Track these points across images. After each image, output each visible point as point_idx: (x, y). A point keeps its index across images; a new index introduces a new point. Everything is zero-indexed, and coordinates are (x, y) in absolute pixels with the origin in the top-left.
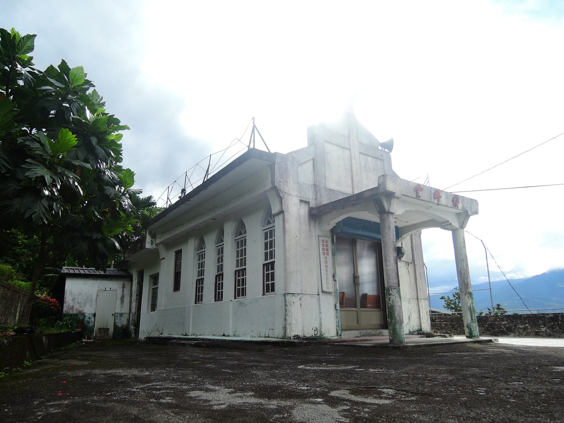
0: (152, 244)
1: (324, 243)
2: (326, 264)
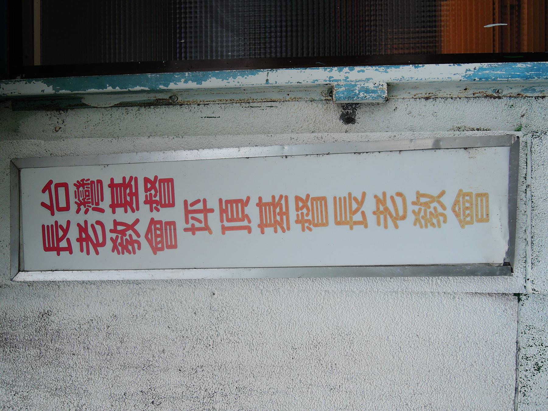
1: (73, 234)
2: (252, 211)
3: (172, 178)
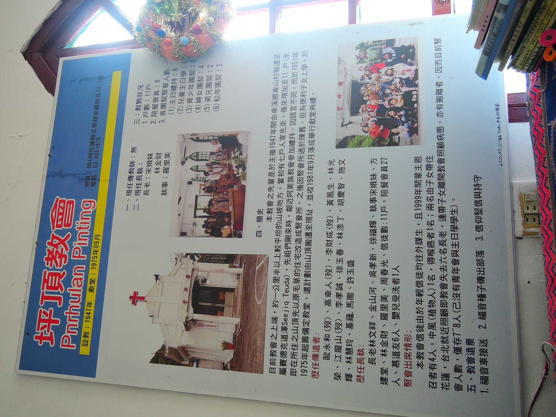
0: (186, 361)
3: (498, 70)
